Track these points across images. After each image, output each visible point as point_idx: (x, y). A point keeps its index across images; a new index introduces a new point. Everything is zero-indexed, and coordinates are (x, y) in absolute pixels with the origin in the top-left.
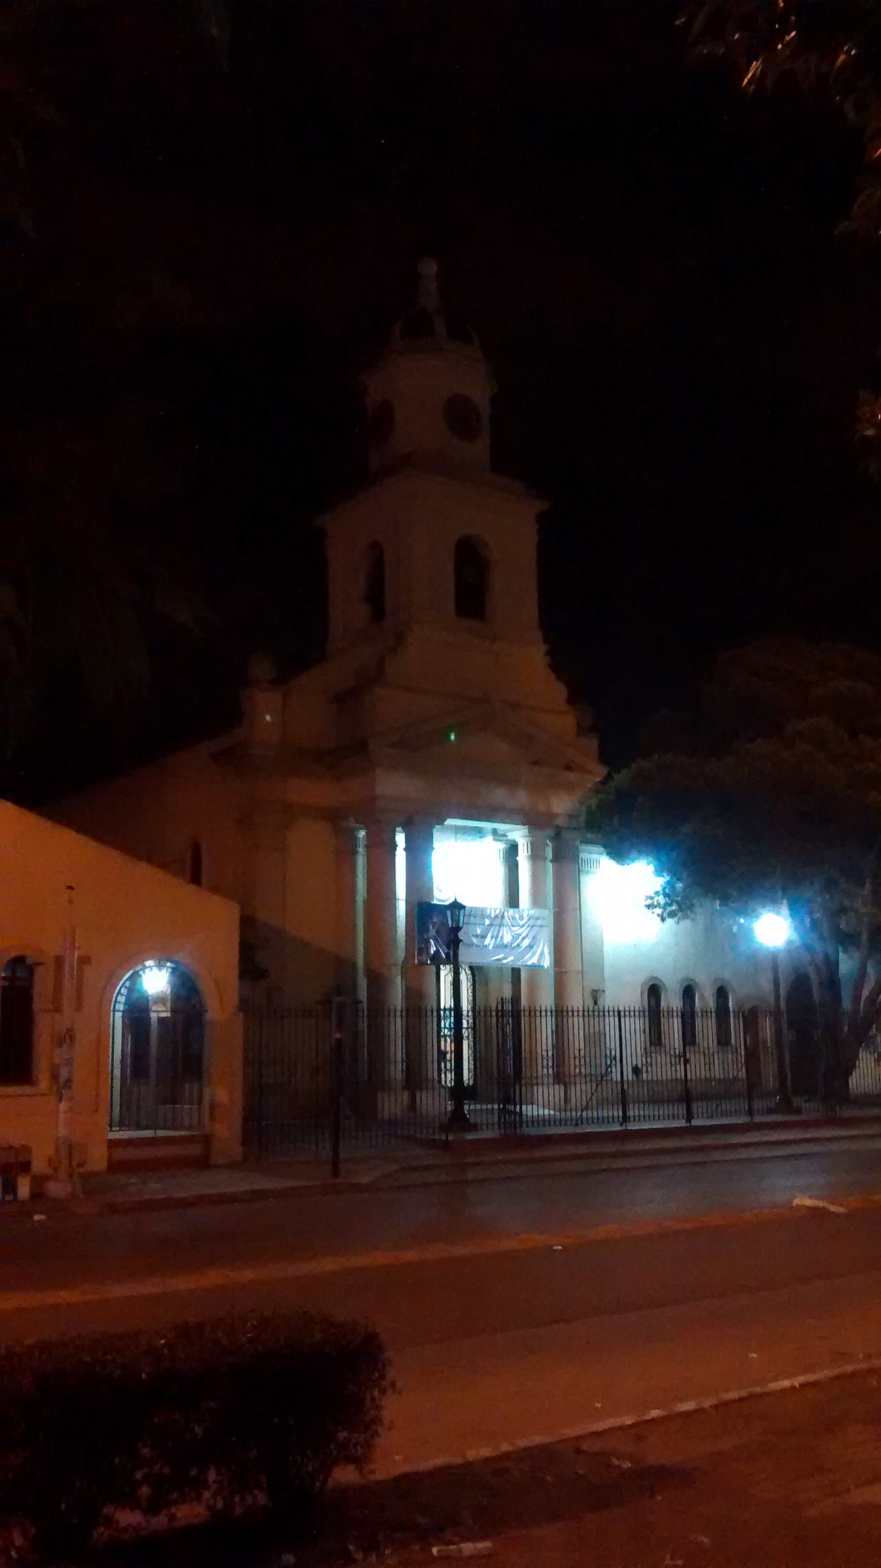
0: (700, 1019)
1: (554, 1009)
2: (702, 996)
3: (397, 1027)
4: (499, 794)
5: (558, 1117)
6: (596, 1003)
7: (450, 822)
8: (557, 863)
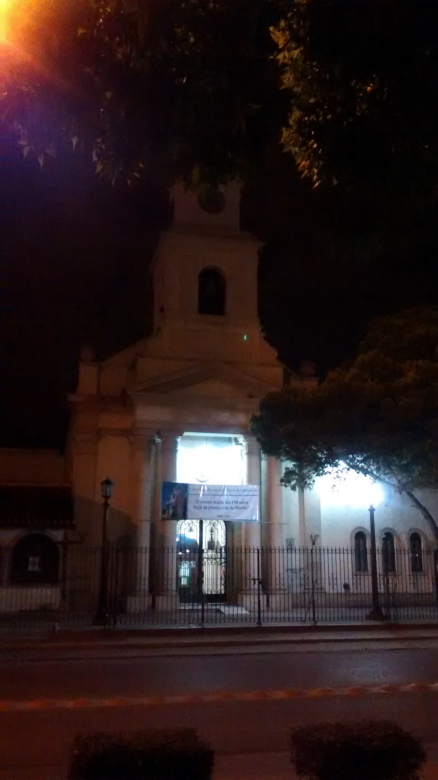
0: (146, 577)
1: (259, 548)
2: (399, 540)
3: (144, 560)
4: (225, 416)
5: (248, 617)
6: (314, 544)
7: (186, 434)
8: (169, 480)
